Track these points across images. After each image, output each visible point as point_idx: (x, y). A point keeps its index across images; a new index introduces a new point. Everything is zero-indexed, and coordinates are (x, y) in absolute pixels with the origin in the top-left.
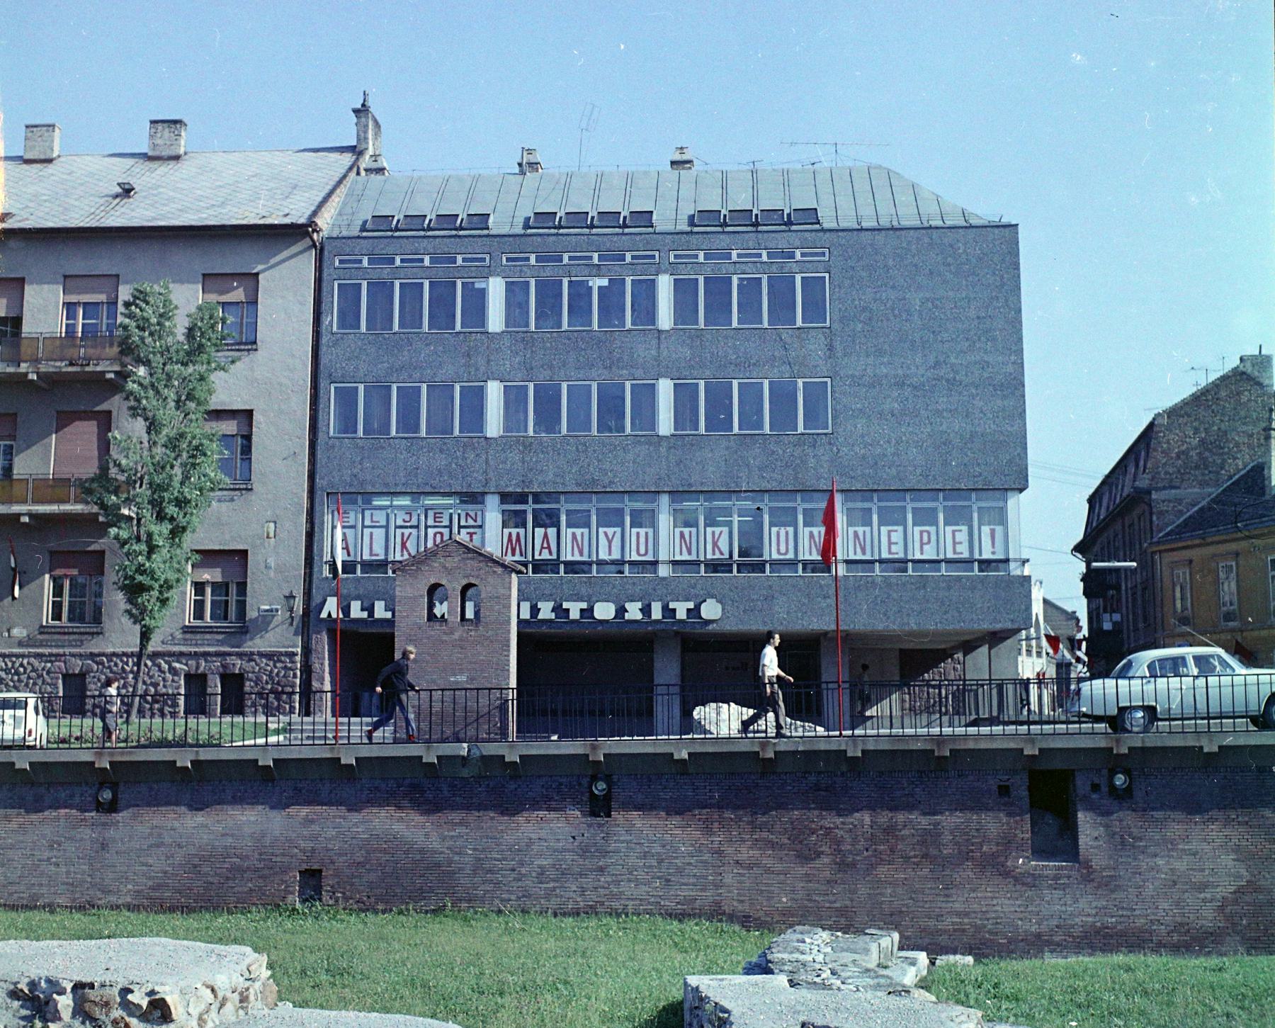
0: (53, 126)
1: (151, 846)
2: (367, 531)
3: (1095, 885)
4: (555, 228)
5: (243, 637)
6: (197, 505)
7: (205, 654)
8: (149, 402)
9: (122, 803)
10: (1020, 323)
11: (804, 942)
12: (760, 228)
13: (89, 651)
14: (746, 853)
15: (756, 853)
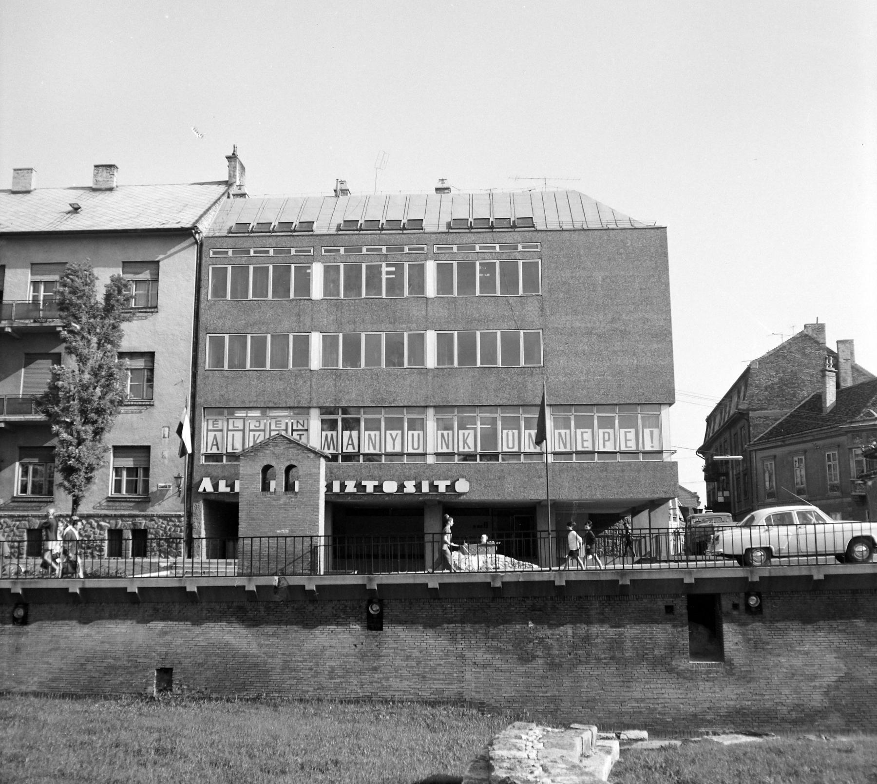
0: (31, 169)
1: (51, 650)
2: (230, 433)
3: (736, 677)
4: (357, 230)
5: (147, 505)
6: (111, 413)
7: (122, 516)
8: (79, 344)
9: (30, 619)
10: (669, 293)
11: (521, 738)
12: (494, 230)
14: (481, 656)
15: (489, 657)
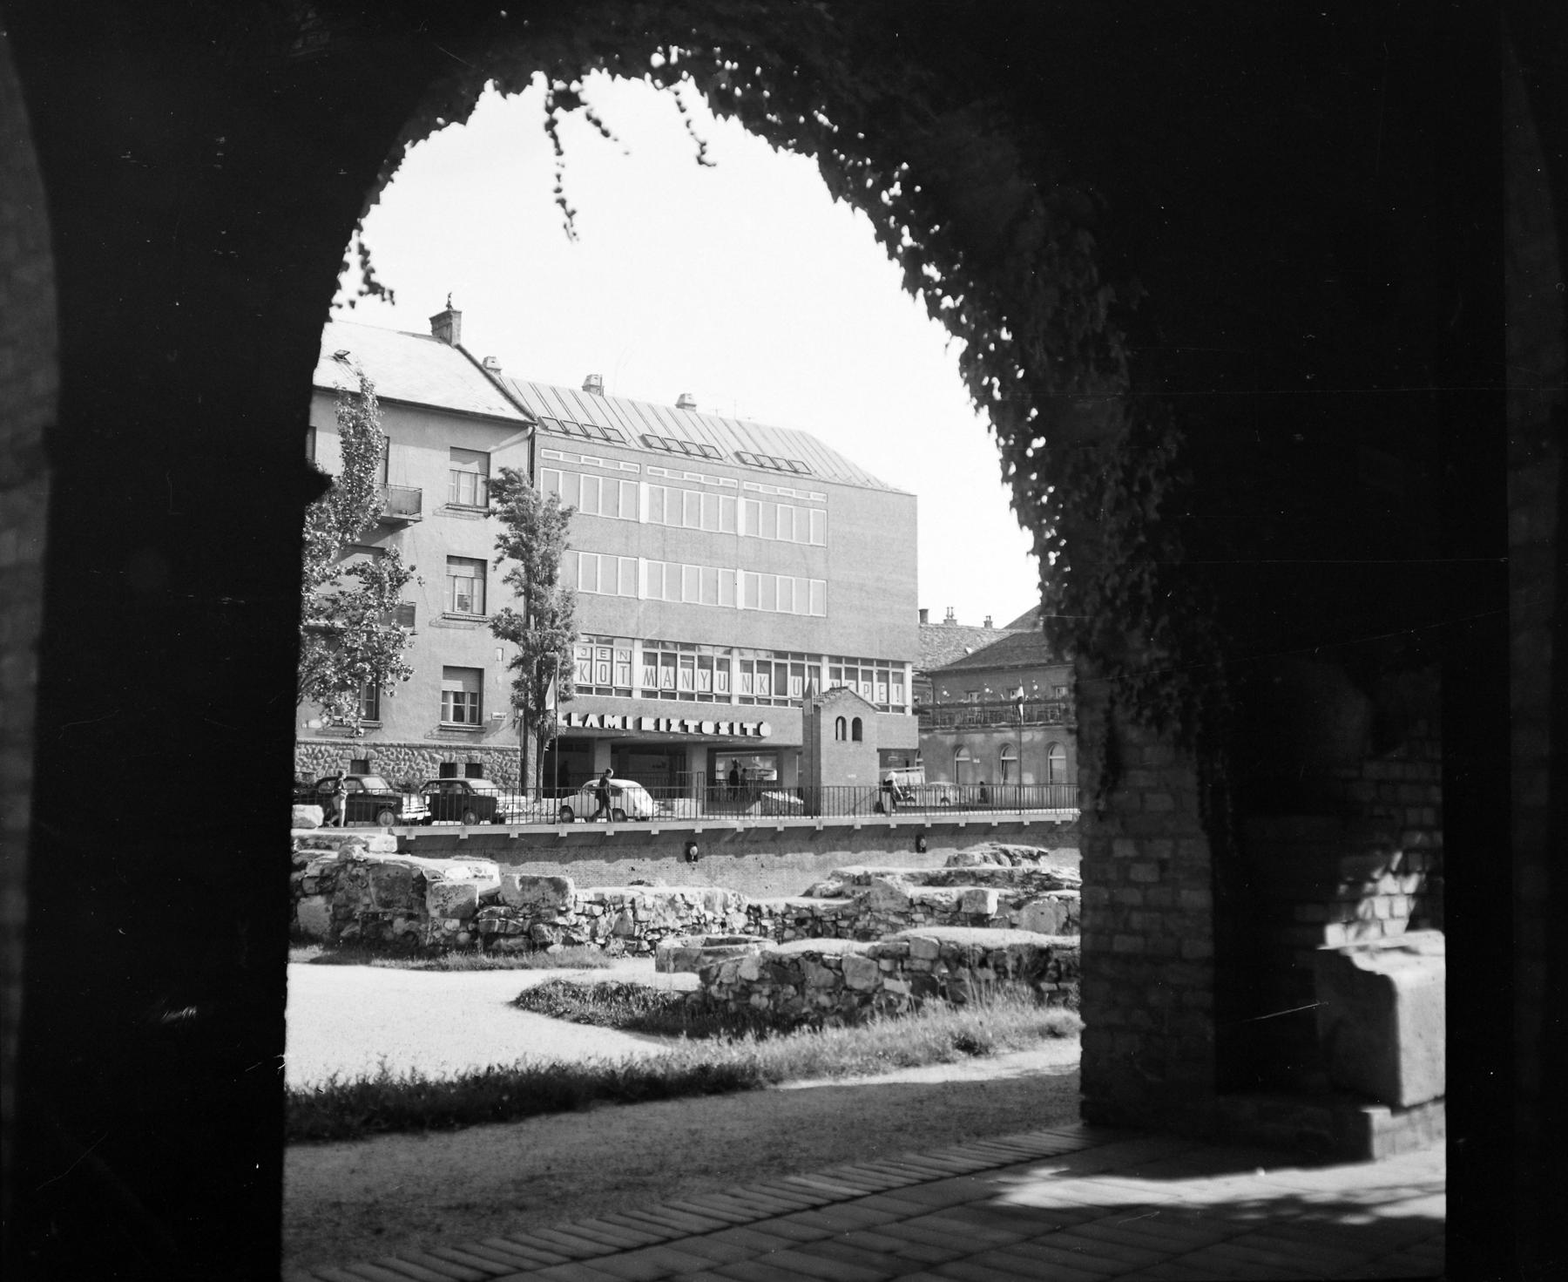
7: (458, 748)
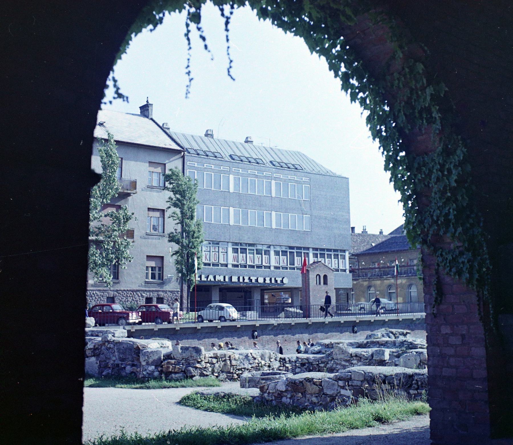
7: (153, 291)
13: (116, 289)
